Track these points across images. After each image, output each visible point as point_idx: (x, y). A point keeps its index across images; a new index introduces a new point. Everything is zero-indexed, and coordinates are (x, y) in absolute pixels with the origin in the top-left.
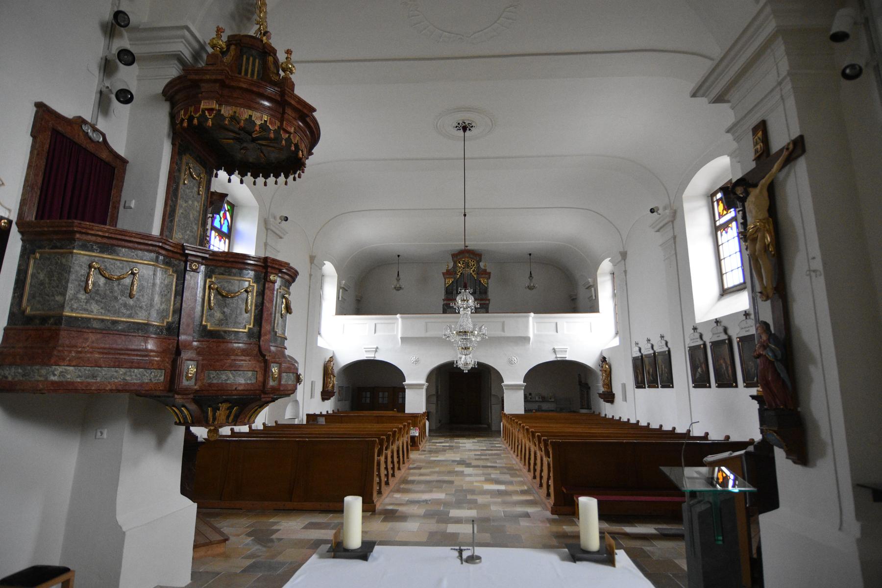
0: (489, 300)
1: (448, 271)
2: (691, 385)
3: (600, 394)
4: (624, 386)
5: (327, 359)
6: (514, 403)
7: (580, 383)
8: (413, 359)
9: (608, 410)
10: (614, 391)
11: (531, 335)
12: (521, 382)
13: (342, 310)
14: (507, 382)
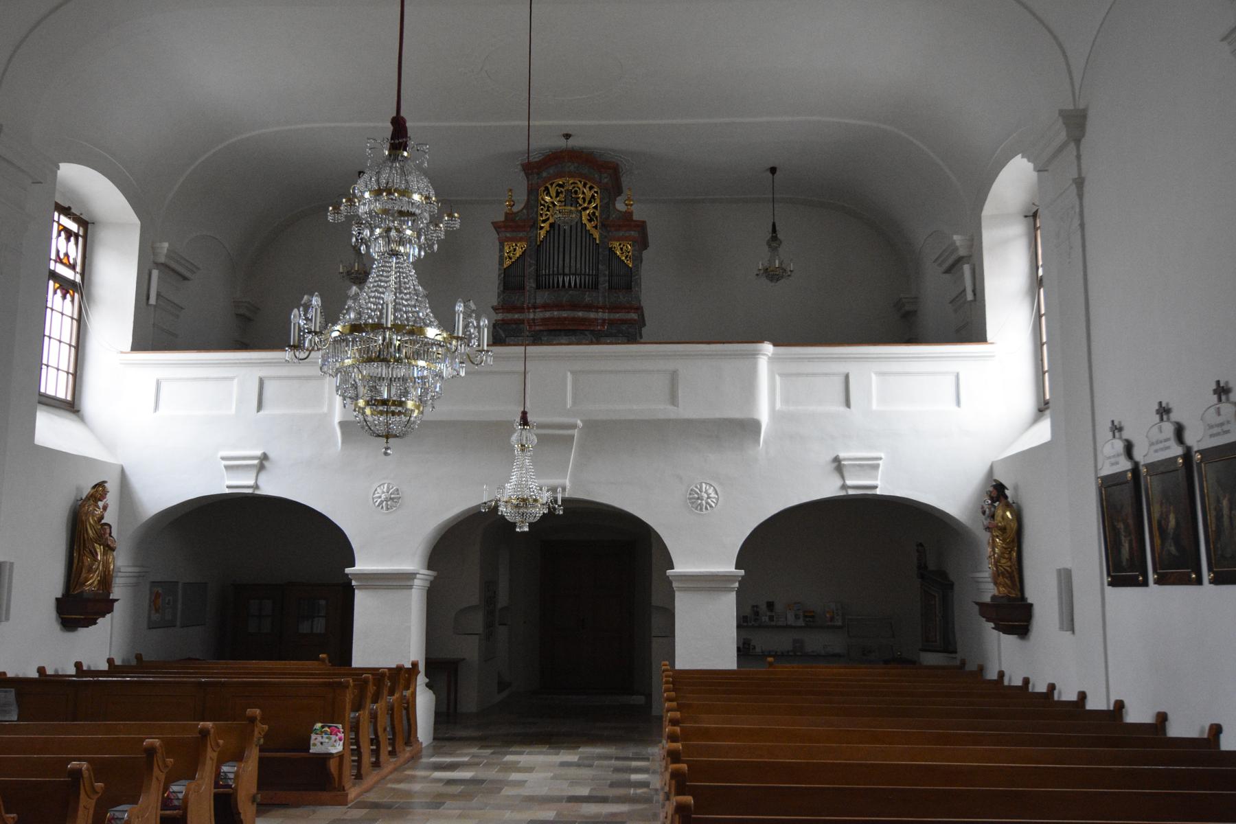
0: (639, 309)
1: (510, 217)
2: (1106, 580)
3: (983, 606)
4: (1065, 579)
5: (87, 490)
6: (705, 636)
7: (922, 571)
8: (382, 493)
9: (1007, 659)
10: (1031, 595)
11: (764, 415)
12: (729, 567)
13: (157, 330)
14: (682, 566)
